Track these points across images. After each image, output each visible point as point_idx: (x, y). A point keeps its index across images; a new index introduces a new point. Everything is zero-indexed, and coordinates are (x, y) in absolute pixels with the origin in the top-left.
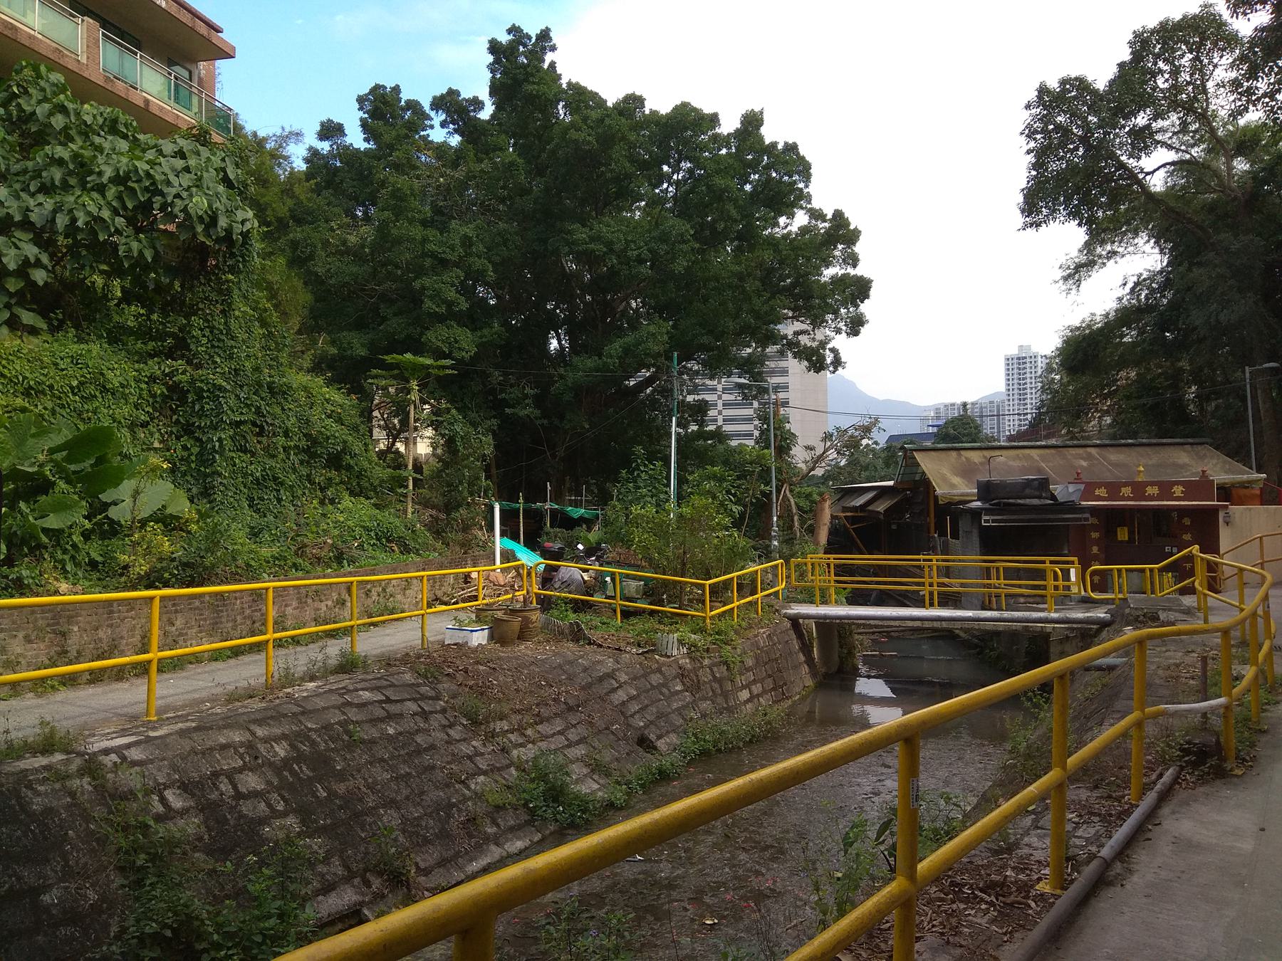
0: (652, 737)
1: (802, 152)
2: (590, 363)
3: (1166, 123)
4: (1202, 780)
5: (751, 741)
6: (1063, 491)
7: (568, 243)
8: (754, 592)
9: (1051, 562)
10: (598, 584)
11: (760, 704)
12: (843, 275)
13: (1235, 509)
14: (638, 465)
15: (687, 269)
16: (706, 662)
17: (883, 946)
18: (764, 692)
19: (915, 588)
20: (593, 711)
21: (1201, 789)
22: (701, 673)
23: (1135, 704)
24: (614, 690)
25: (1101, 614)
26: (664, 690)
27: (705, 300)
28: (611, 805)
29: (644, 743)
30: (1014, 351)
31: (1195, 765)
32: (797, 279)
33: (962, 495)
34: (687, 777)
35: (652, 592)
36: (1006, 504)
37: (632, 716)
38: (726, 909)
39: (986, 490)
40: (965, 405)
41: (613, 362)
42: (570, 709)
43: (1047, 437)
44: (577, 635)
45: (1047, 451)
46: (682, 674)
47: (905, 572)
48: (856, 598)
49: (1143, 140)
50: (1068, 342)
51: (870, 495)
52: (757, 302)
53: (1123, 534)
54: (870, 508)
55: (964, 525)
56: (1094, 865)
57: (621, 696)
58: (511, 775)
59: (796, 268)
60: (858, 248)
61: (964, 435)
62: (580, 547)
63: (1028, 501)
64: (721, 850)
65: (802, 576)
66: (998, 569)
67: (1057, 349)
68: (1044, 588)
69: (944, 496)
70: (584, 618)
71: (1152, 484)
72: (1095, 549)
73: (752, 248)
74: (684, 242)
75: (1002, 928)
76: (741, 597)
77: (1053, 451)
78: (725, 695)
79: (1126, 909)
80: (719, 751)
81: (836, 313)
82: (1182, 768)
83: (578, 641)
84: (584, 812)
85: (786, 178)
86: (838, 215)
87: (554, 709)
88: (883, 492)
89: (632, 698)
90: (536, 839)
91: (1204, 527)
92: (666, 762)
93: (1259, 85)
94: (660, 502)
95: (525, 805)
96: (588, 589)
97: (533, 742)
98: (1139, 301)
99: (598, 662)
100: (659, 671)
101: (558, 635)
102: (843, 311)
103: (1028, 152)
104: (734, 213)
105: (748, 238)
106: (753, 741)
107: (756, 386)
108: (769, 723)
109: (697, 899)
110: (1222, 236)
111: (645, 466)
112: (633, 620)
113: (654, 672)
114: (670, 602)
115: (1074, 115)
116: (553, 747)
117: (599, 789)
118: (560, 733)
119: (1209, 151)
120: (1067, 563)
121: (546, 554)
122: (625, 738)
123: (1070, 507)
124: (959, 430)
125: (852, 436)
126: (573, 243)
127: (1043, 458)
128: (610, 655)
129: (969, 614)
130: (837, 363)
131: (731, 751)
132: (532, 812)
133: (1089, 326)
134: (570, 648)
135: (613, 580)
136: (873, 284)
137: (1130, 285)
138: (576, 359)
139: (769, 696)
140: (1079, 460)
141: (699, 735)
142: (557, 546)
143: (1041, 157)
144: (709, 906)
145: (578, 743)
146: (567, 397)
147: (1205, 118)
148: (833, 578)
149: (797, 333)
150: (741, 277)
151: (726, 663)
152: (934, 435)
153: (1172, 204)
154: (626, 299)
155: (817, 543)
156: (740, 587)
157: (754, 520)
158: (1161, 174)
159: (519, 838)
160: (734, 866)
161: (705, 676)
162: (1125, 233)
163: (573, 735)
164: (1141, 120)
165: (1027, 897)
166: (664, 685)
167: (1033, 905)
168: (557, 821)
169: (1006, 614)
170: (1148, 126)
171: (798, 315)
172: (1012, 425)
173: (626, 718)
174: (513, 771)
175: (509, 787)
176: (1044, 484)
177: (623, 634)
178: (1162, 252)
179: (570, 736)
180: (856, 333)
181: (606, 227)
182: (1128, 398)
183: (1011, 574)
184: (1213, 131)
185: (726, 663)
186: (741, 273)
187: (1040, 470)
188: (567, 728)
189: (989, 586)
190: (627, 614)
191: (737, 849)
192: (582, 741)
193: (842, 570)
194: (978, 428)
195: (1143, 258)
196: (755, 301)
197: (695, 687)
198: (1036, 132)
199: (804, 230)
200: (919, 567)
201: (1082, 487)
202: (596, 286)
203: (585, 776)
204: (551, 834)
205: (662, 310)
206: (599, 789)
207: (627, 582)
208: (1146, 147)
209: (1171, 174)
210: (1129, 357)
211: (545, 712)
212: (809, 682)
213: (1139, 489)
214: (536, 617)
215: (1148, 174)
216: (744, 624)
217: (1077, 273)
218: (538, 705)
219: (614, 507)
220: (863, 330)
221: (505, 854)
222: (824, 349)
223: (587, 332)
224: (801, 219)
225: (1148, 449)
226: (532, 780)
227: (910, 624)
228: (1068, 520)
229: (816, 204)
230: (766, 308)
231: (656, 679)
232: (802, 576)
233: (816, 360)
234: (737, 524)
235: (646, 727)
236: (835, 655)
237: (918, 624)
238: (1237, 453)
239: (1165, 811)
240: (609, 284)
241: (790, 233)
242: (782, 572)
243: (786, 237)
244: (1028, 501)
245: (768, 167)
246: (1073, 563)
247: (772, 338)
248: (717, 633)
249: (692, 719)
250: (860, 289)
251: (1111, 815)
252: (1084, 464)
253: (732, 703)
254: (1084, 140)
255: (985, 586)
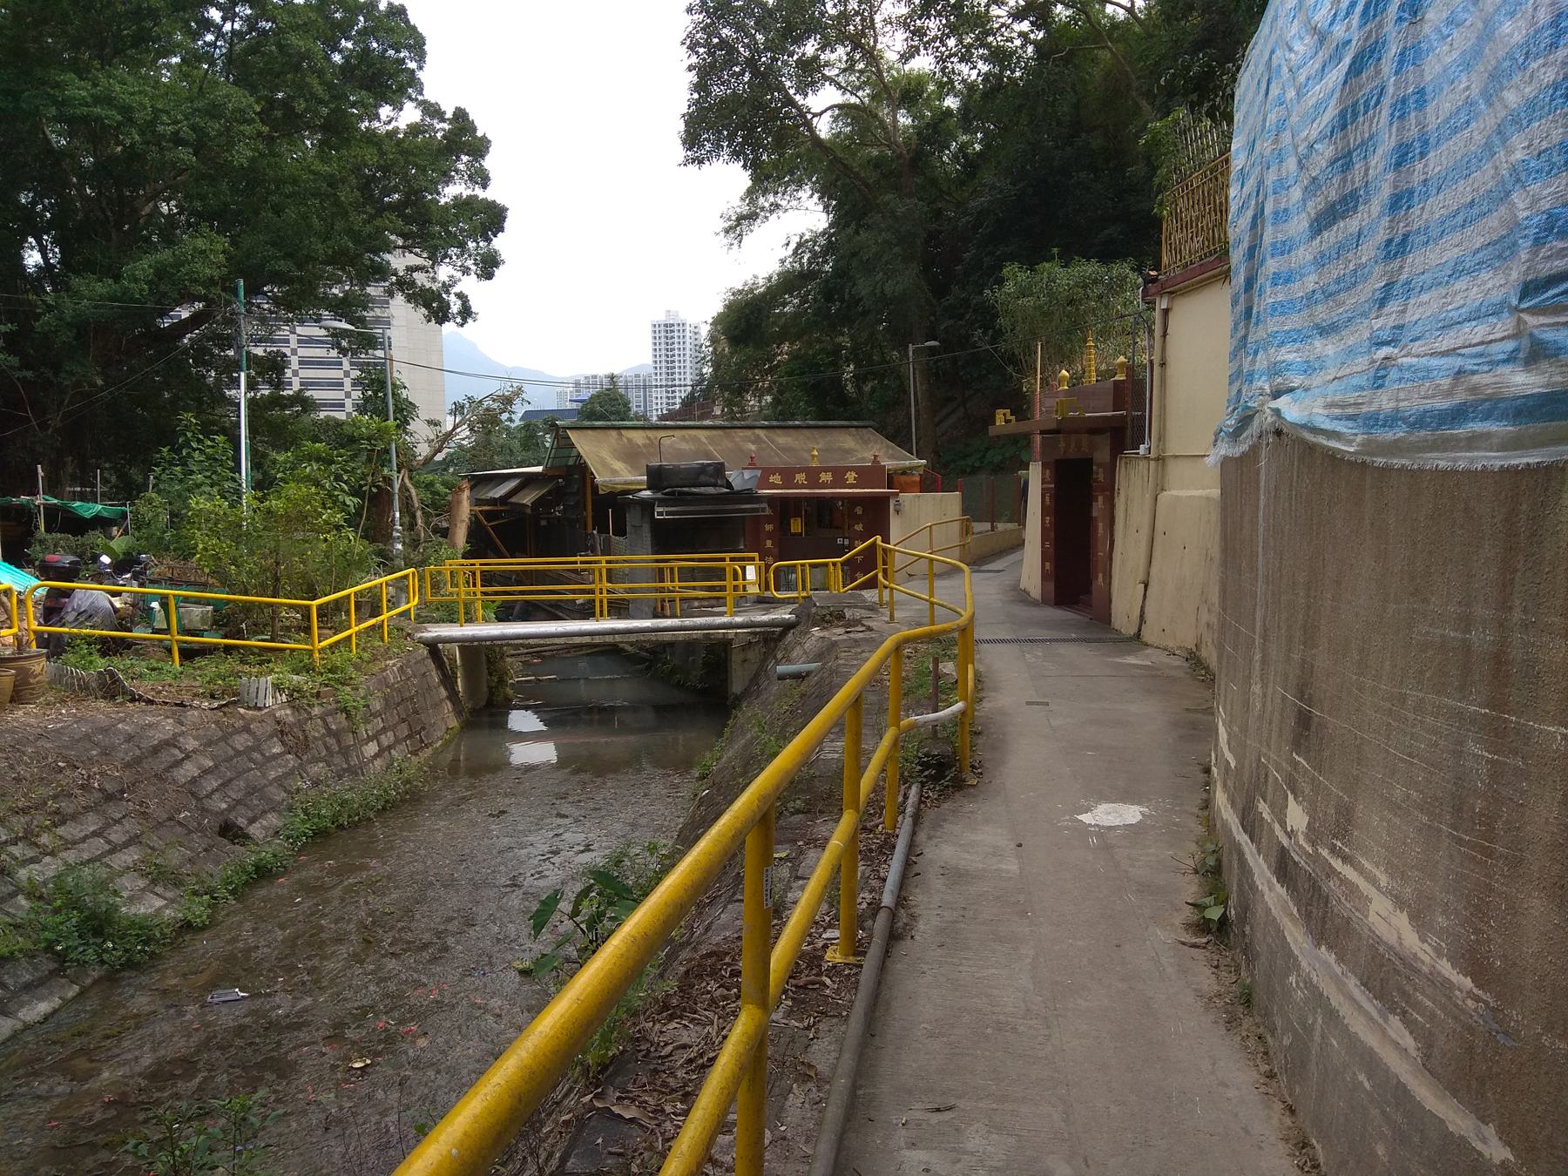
0: (241, 822)
1: (413, 19)
2: (102, 288)
3: (833, 57)
4: (944, 795)
5: (384, 808)
6: (739, 478)
7: (55, 102)
8: (375, 612)
9: (732, 559)
10: (140, 612)
11: (392, 760)
12: (470, 197)
13: (906, 497)
14: (187, 442)
15: (252, 160)
16: (316, 711)
17: (672, 1082)
18: (398, 741)
19: (571, 596)
20: (146, 796)
21: (946, 806)
22: (308, 726)
23: (889, 717)
24: (178, 763)
25: (784, 614)
26: (256, 755)
27: (278, 210)
28: (187, 926)
29: (229, 831)
30: (661, 318)
31: (935, 779)
32: (407, 195)
33: (626, 483)
34: (298, 869)
35: (225, 620)
36: (681, 493)
37: (209, 796)
38: (380, 1041)
39: (657, 477)
40: (612, 377)
41: (139, 289)
42: (109, 797)
43: (701, 418)
44: (111, 689)
45: (714, 432)
46: (282, 731)
47: (557, 578)
48: (505, 614)
49: (810, 72)
50: (730, 307)
51: (512, 484)
52: (357, 219)
53: (796, 526)
54: (513, 500)
55: (632, 518)
56: (882, 917)
57: (190, 770)
58: (20, 907)
59: (406, 179)
60: (488, 163)
61: (612, 413)
62: (105, 559)
63: (702, 490)
64: (361, 962)
65: (436, 586)
66: (672, 569)
67: (719, 315)
68: (723, 589)
69: (604, 484)
70: (119, 664)
71: (826, 470)
72: (769, 543)
73: (347, 142)
74: (250, 122)
75: (802, 1020)
76: (359, 621)
77: (720, 432)
78: (345, 752)
79: (925, 967)
80: (341, 827)
81: (462, 246)
82: (923, 784)
83: (113, 697)
84: (146, 943)
85: (391, 52)
86: (460, 115)
87: (83, 801)
88: (528, 481)
89: (206, 772)
90: (70, 994)
91: (875, 514)
92: (266, 855)
93: (931, 25)
94: (220, 498)
95: (49, 948)
96: (122, 621)
97: (52, 854)
98: (801, 265)
99: (150, 726)
100: (246, 729)
101: (82, 691)
102: (471, 245)
103: (690, 68)
104: (319, 90)
105: (338, 130)
106: (388, 808)
107: (362, 340)
108: (408, 782)
109: (336, 1036)
110: (888, 197)
111: (199, 441)
112: (200, 662)
113: (238, 732)
114: (256, 633)
115: (740, 27)
116: (86, 856)
117: (166, 907)
118: (95, 834)
119: (873, 97)
120: (743, 559)
121: (46, 571)
122: (201, 829)
123: (748, 496)
124: (606, 406)
125: (487, 409)
126: (64, 103)
127: (711, 440)
128: (168, 713)
129: (647, 623)
130: (466, 313)
131: (356, 825)
132: (61, 958)
133: (752, 290)
134: (101, 710)
135: (165, 605)
136: (509, 213)
137: (793, 246)
138: (75, 281)
139: (402, 747)
140: (746, 442)
141: (311, 810)
142: (67, 560)
143: (705, 76)
144: (354, 1043)
145: (126, 845)
146: (66, 336)
147: (872, 57)
148: (479, 588)
149: (411, 269)
150: (332, 182)
151: (345, 710)
152: (579, 412)
153: (840, 154)
154: (155, 197)
155: (453, 545)
156: (358, 606)
157: (372, 511)
158: (827, 117)
159: (41, 999)
160: (385, 980)
161: (315, 730)
162: (787, 184)
163: (117, 835)
164: (810, 48)
165: (819, 974)
166: (252, 749)
167: (828, 981)
168: (102, 962)
169: (688, 622)
170: (816, 58)
171: (412, 241)
172: (658, 405)
173: (199, 800)
174: (22, 900)
175: (16, 926)
176: (719, 469)
177: (185, 682)
178: (826, 207)
179: (114, 837)
180: (489, 276)
181: (120, 82)
182: (790, 374)
183: (688, 574)
184: (879, 73)
185: (345, 710)
186: (332, 176)
187: (708, 455)
188: (107, 826)
189: (662, 590)
190: (188, 654)
191: (383, 956)
192: (133, 840)
193: (488, 579)
194: (626, 404)
195: (804, 216)
196: (353, 216)
197: (299, 746)
198: (698, 44)
199: (414, 129)
200: (575, 571)
201: (759, 473)
202: (104, 172)
203: (143, 890)
204: (95, 982)
205: (220, 218)
206: (166, 907)
207: (186, 608)
208: (813, 83)
209: (835, 119)
210: (793, 329)
211: (67, 806)
212: (454, 723)
213: (813, 476)
214: (41, 667)
215: (815, 115)
216: (366, 656)
217: (740, 224)
218: (55, 797)
219: (150, 501)
220: (497, 272)
221: (19, 1026)
222: (448, 293)
223: (84, 242)
224: (410, 114)
225: (815, 432)
226: (57, 911)
227: (578, 640)
228: (745, 511)
229: (430, 95)
230: (368, 229)
231: (241, 741)
232: (436, 586)
233: (436, 307)
234: (352, 522)
235: (231, 809)
236: (484, 686)
237: (587, 639)
238: (898, 437)
239: (922, 836)
240: (126, 176)
241: (396, 131)
242: (413, 583)
243: (392, 134)
244: (702, 490)
245: (364, 32)
246: (753, 559)
247: (380, 272)
248: (330, 671)
249: (298, 790)
250: (492, 219)
251: (871, 851)
252: (753, 447)
253: (354, 761)
254: (751, 63)
255: (657, 590)
